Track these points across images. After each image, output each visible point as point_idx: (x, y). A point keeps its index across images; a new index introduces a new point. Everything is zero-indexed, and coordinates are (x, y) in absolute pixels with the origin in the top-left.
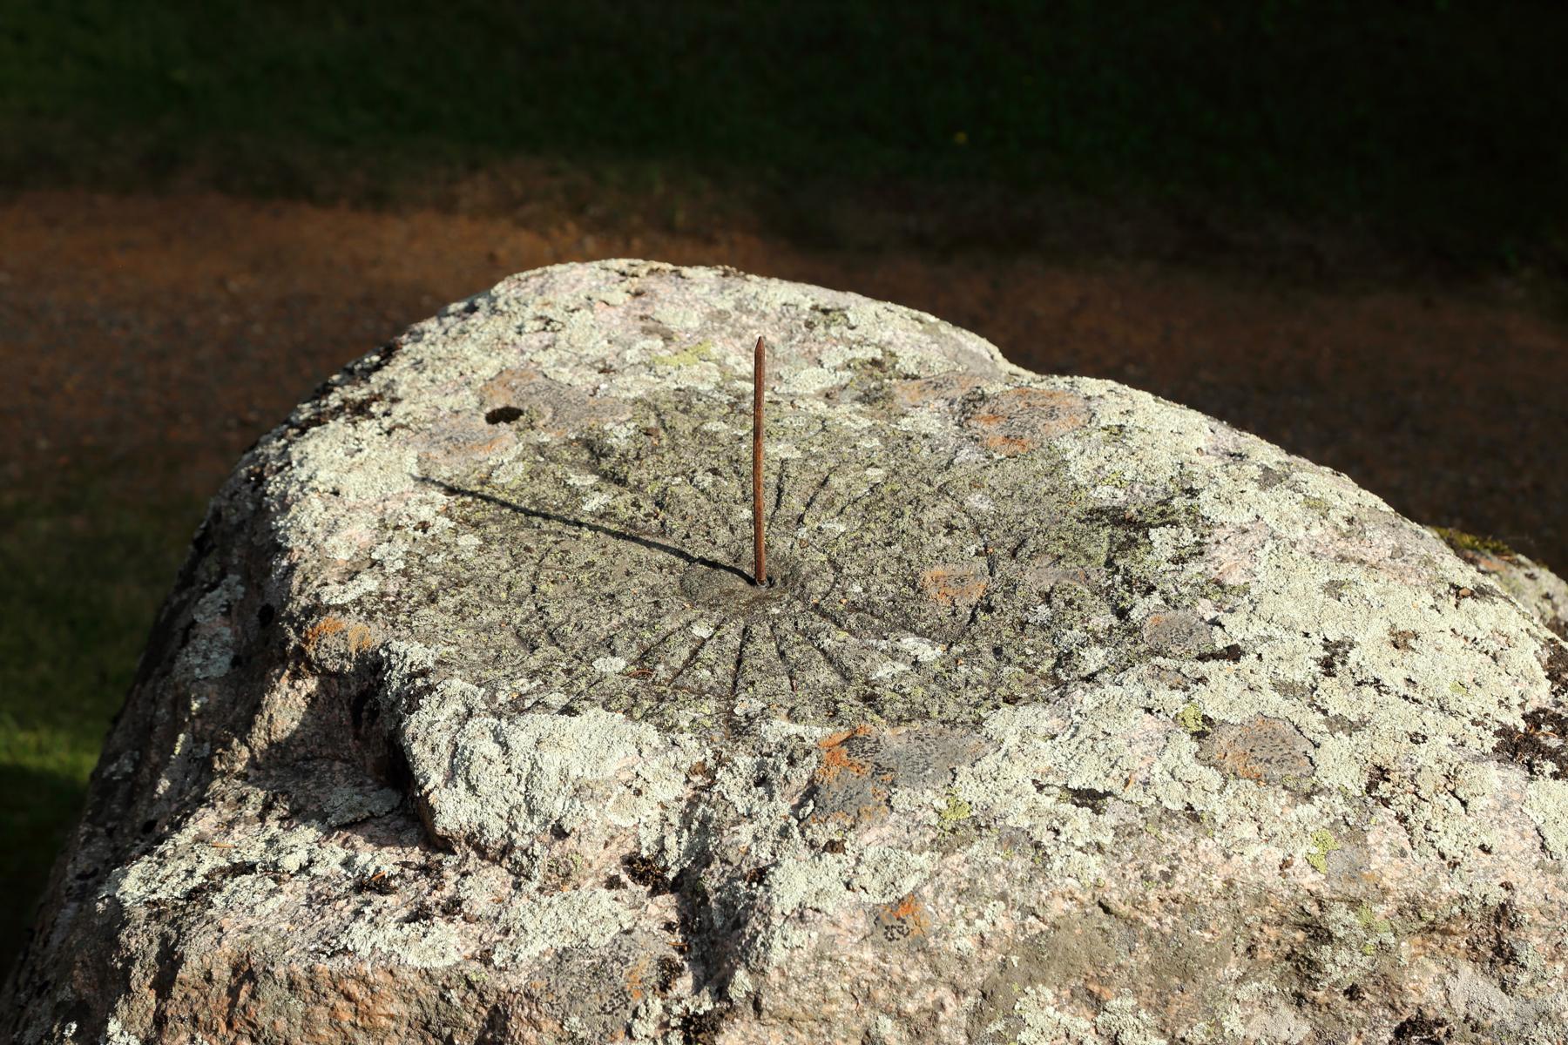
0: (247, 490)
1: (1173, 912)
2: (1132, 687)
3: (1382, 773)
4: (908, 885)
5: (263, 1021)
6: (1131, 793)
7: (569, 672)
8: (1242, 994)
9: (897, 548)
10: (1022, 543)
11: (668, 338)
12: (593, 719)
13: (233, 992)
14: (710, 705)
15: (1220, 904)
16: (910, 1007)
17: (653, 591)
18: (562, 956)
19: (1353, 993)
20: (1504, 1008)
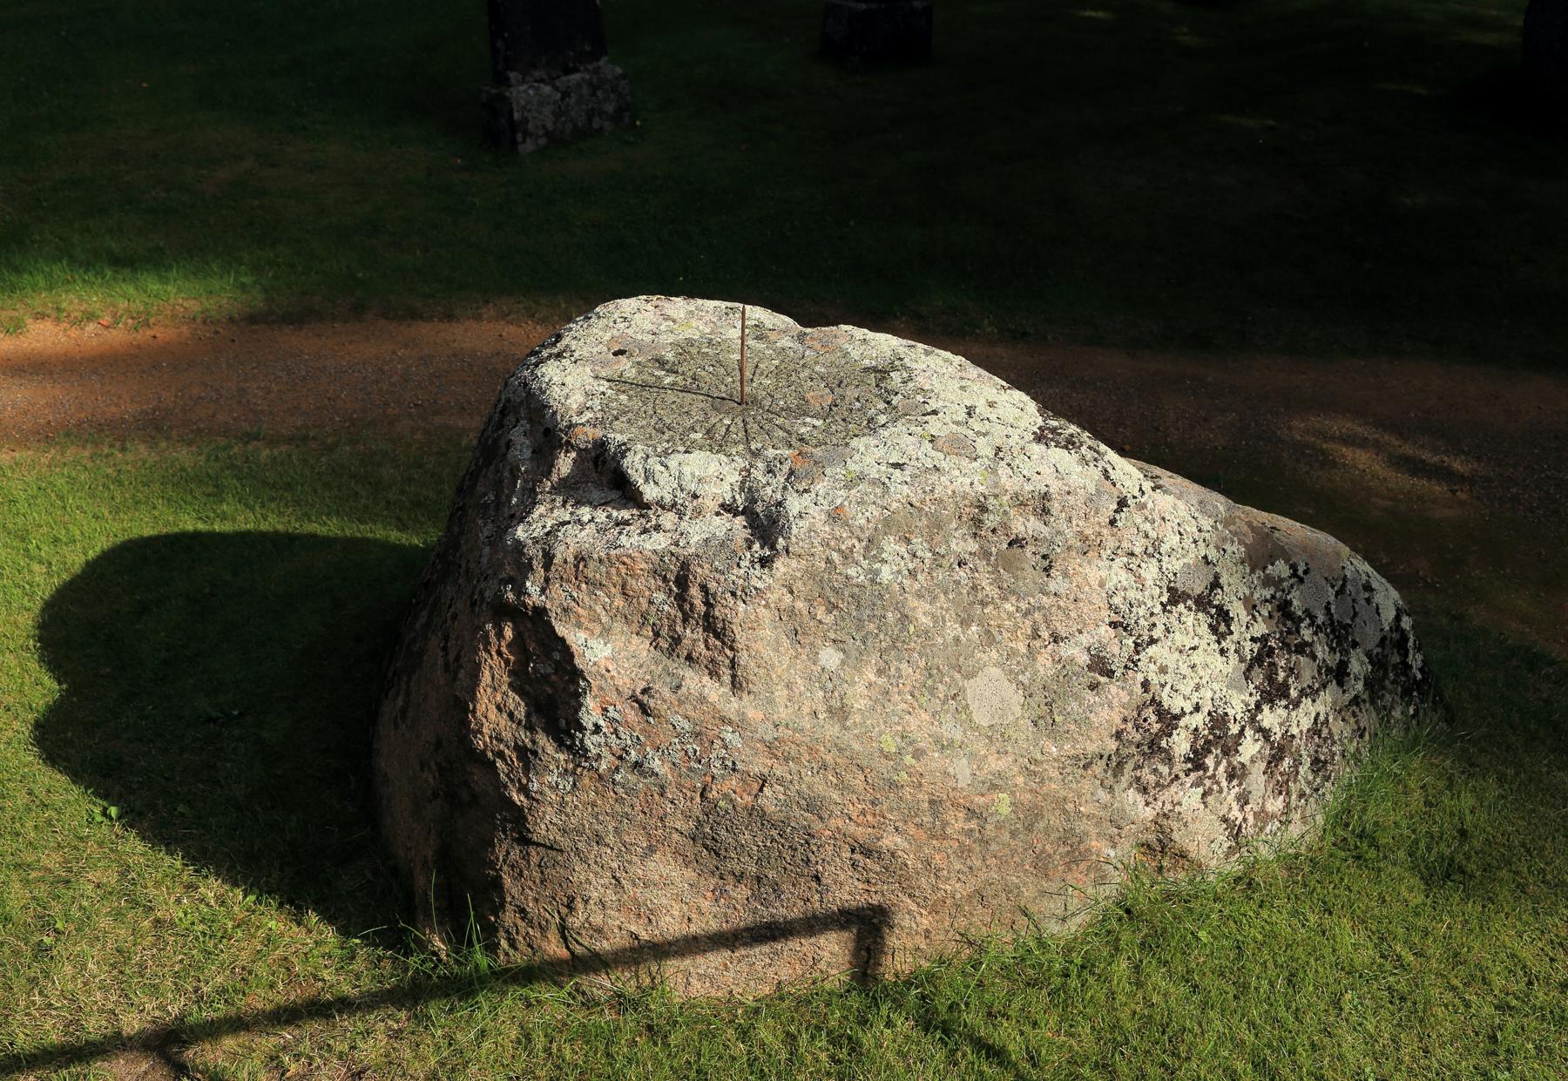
0: (521, 389)
1: (934, 504)
2: (900, 427)
3: (999, 449)
4: (839, 502)
5: (590, 576)
6: (912, 463)
7: (681, 439)
8: (956, 535)
9: (793, 387)
10: (841, 382)
11: (674, 321)
12: (697, 456)
13: (577, 567)
14: (741, 447)
15: (951, 500)
16: (843, 547)
17: (702, 409)
18: (706, 541)
19: (994, 531)
20: (1046, 531)
